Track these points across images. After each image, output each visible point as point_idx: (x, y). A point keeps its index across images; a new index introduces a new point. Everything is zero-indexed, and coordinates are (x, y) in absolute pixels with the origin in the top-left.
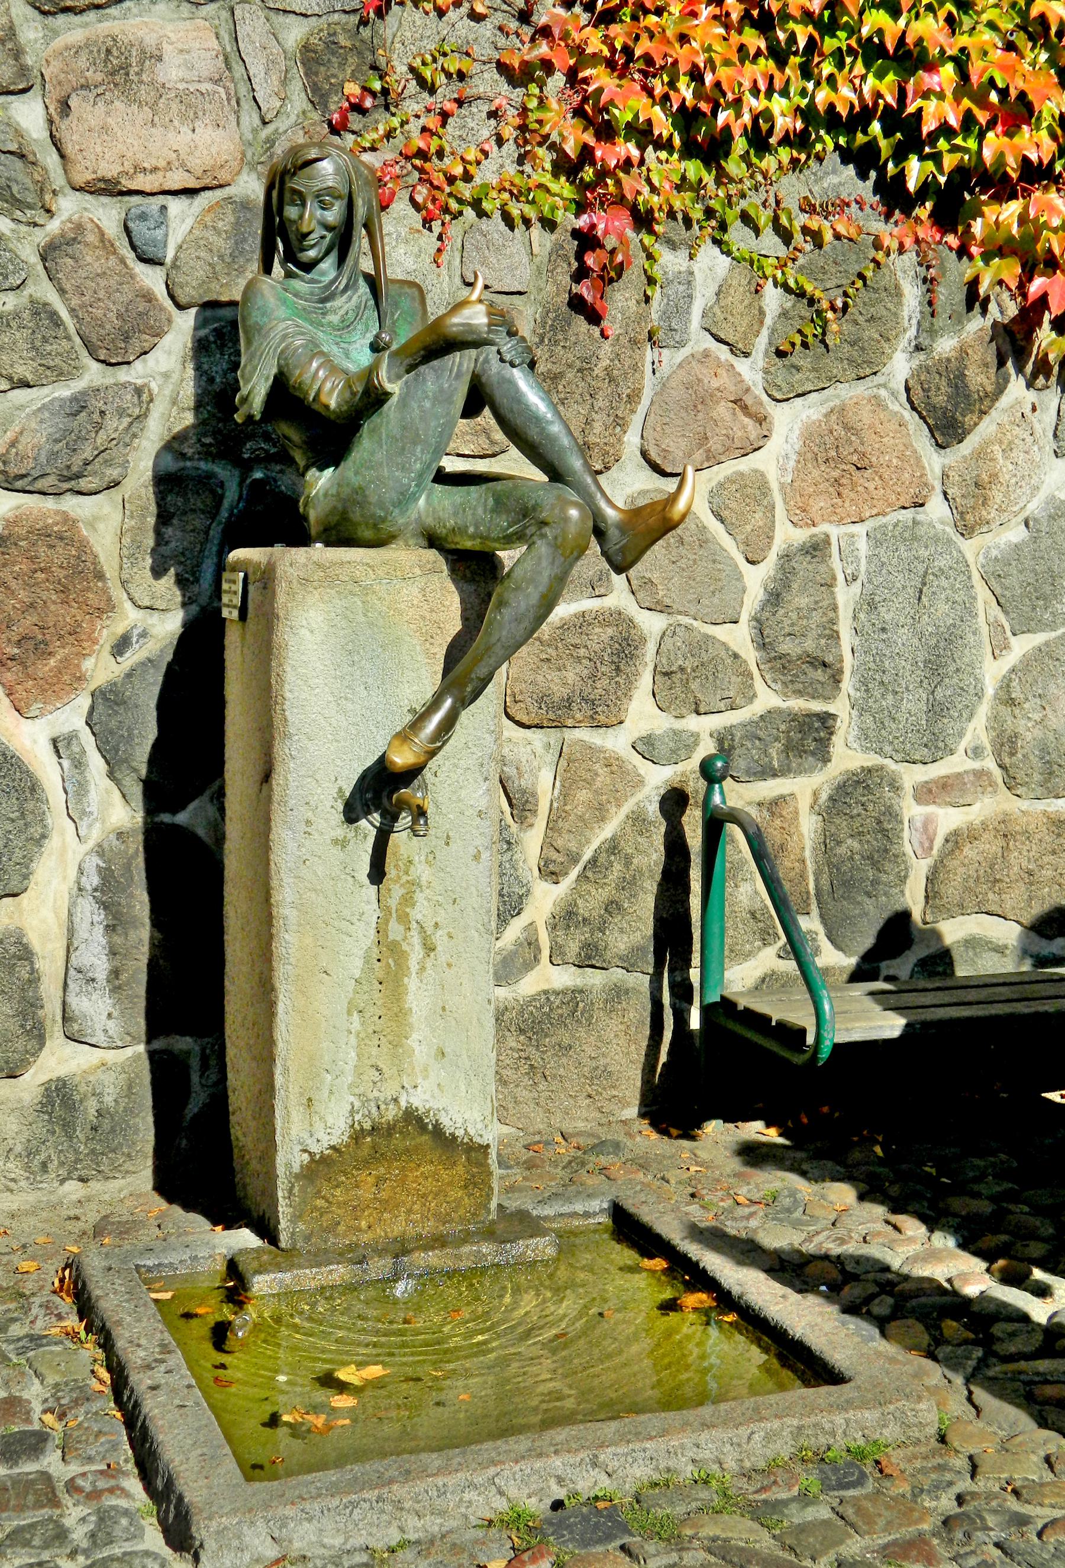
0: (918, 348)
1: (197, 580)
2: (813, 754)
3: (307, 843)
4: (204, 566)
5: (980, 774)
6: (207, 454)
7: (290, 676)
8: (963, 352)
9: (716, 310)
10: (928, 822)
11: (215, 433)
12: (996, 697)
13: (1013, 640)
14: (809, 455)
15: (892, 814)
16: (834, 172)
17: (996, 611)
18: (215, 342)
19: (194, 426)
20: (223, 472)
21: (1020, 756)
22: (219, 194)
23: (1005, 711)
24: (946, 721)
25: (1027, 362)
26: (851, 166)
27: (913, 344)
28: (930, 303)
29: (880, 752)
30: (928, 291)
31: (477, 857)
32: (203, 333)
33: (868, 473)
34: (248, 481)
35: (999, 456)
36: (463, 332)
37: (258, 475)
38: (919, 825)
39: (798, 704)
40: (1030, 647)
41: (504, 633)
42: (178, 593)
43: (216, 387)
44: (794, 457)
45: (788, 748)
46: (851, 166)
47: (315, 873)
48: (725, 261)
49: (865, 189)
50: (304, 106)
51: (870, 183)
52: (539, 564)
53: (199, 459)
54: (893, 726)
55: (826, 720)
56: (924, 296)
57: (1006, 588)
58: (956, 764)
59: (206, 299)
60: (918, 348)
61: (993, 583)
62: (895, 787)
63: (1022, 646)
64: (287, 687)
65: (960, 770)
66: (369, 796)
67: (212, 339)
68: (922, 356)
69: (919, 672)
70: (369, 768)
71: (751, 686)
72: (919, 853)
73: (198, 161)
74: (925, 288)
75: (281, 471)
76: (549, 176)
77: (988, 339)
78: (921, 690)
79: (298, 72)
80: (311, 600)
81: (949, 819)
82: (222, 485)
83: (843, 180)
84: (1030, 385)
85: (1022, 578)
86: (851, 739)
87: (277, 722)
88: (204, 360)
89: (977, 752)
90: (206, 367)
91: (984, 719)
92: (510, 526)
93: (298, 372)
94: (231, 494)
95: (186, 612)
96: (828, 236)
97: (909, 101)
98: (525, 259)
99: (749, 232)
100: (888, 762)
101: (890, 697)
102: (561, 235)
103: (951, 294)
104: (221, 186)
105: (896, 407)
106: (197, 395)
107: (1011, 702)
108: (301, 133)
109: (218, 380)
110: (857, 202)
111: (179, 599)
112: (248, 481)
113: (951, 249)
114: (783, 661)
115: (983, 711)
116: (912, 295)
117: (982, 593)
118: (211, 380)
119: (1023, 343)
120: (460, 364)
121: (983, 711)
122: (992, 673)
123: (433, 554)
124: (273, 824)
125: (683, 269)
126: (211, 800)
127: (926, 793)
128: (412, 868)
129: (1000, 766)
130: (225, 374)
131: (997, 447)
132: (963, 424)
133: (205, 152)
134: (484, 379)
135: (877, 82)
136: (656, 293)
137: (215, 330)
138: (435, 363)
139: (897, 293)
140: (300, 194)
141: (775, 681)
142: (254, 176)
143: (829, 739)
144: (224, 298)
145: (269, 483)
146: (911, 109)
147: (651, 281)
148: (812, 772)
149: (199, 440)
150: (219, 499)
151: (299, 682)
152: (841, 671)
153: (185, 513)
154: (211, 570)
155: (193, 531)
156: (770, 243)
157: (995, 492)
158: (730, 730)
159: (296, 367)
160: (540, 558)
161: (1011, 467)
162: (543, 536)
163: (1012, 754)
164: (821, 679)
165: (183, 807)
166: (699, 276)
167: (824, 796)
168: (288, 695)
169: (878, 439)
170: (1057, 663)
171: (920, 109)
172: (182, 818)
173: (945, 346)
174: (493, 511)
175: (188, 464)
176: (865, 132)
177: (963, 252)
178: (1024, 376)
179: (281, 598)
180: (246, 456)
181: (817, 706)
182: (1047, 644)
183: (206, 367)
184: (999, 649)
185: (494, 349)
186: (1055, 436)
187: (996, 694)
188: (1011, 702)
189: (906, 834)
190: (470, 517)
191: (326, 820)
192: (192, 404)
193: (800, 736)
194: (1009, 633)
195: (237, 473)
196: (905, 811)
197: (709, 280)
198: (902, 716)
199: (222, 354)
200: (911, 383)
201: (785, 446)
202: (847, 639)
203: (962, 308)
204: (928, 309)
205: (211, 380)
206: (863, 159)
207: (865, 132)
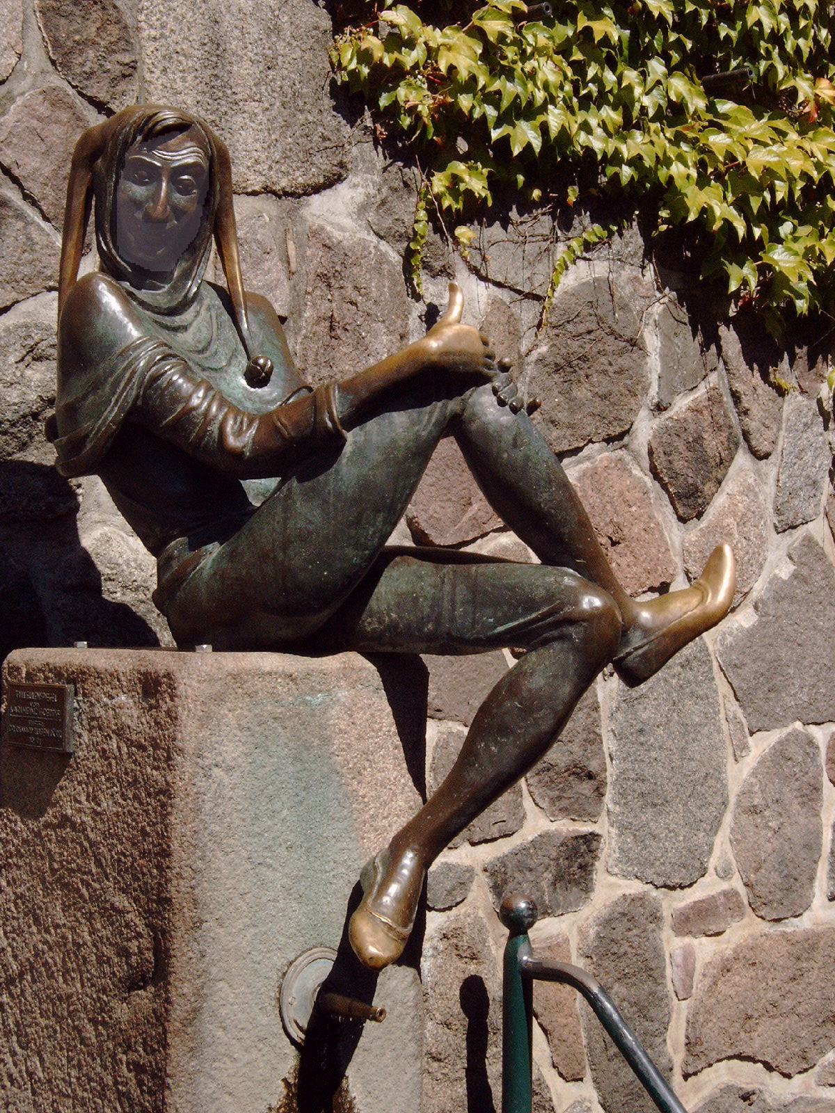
5: (731, 895)
10: (688, 955)
13: (750, 739)
17: (734, 707)
19: (784, 582)
33: (620, 548)
38: (679, 960)
39: (566, 827)
45: (558, 879)
50: (43, 65)
55: (594, 837)
58: (707, 888)
61: (730, 674)
62: (656, 918)
63: (761, 745)
71: (521, 805)
79: (36, 21)
81: (706, 949)
85: (755, 667)
89: (725, 874)
98: (283, 276)
105: (637, 472)
114: (552, 773)
117: (722, 687)
127: (690, 922)
129: (746, 885)
141: (543, 798)
143: (593, 865)
152: (603, 783)
158: (503, 861)
164: (586, 792)
169: (627, 509)
181: (585, 828)
182: (780, 743)
184: (741, 749)
189: (668, 972)
193: (566, 863)
194: (748, 734)
196: (665, 944)
202: (609, 744)
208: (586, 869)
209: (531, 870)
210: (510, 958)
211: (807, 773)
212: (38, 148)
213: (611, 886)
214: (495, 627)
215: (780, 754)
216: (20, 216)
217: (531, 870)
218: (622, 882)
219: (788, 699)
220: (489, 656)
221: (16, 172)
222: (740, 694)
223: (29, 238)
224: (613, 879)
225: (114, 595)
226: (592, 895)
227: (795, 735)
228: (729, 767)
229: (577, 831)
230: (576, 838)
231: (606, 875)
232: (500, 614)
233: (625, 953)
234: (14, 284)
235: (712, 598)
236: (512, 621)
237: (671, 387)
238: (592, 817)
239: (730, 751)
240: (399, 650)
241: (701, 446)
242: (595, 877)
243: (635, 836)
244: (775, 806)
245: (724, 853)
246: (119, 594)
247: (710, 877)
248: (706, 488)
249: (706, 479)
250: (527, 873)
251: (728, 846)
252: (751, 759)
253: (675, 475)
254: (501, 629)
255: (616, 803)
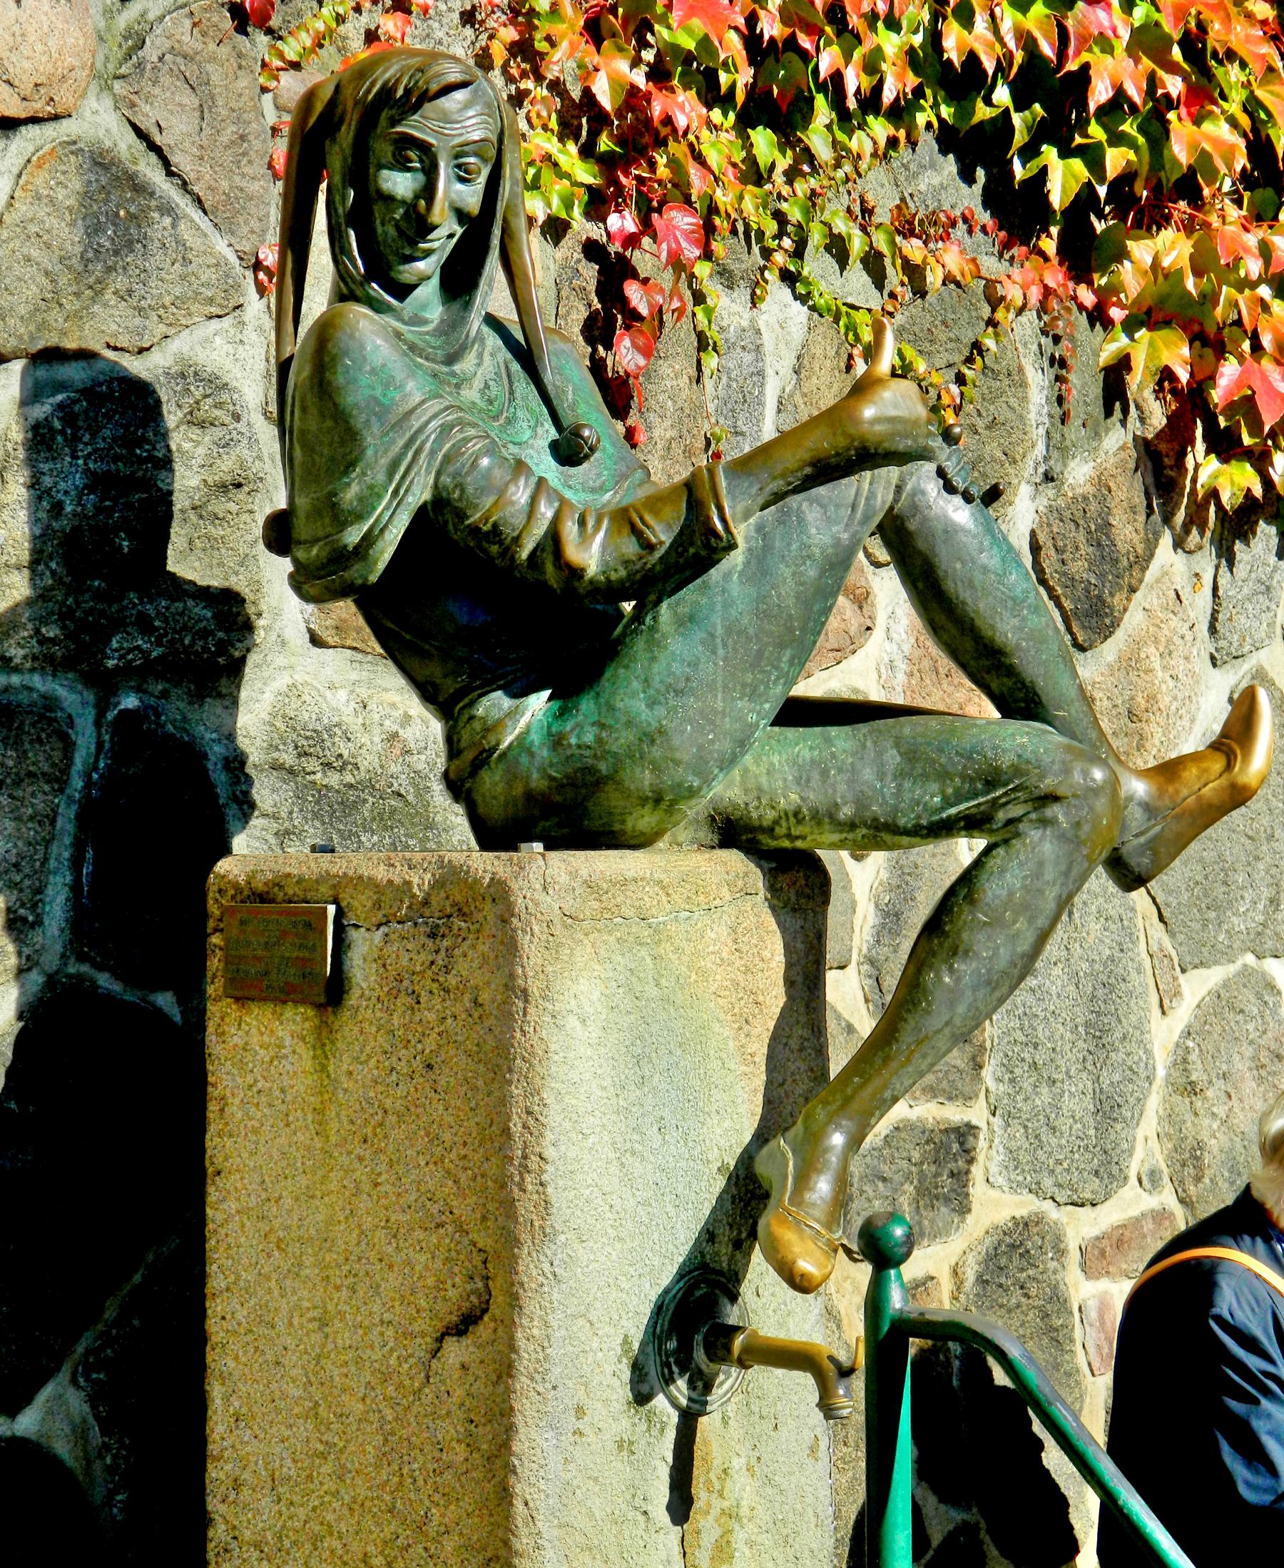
0: (1048, 478)
1: (38, 922)
2: (947, 1200)
3: (578, 1452)
4: (50, 891)
6: (47, 662)
7: (554, 1117)
8: (1102, 485)
9: (798, 399)
11: (64, 617)
12: (1169, 1081)
13: (1182, 979)
14: (926, 663)
15: (1058, 1299)
16: (933, 166)
18: (63, 432)
19: (29, 602)
20: (70, 696)
21: (1207, 1180)
22: (49, 132)
23: (1182, 1103)
24: (1118, 1127)
25: (1177, 505)
26: (951, 156)
27: (1041, 470)
28: (1060, 400)
29: (1036, 1190)
30: (1058, 378)
31: (813, 1450)
32: (41, 411)
34: (110, 716)
35: (1156, 663)
36: (893, 435)
37: (130, 702)
38: (1093, 1314)
40: (1204, 992)
41: (961, 1009)
42: (11, 948)
43: (63, 524)
44: (902, 666)
46: (951, 156)
47: (591, 1515)
48: (799, 312)
49: (969, 198)
51: (978, 188)
52: (1038, 874)
53: (32, 670)
54: (1054, 1141)
55: (965, 1133)
56: (1052, 387)
57: (1170, 892)
59: (41, 345)
60: (1048, 478)
63: (1197, 986)
64: (549, 1136)
65: (1134, 1212)
66: (672, 1345)
67: (57, 424)
68: (1050, 490)
69: (1081, 1044)
70: (666, 1291)
72: (1096, 1366)
73: (27, 65)
74: (1051, 373)
75: (165, 695)
76: (555, 139)
77: (1132, 465)
78: (1084, 1075)
80: (583, 954)
82: (70, 721)
83: (941, 183)
84: (1178, 544)
86: (994, 1169)
87: (525, 1208)
88: (45, 467)
89: (1151, 1180)
90: (47, 481)
91: (1155, 1121)
92: (947, 803)
93: (488, 502)
94: (85, 739)
95: (22, 986)
96: (934, 278)
97: (1071, 51)
99: (830, 263)
100: (1048, 1206)
101: (1044, 1090)
102: (570, 248)
103: (1085, 387)
104: (56, 117)
106: (34, 539)
107: (1192, 1089)
108: (188, 23)
109: (69, 509)
110: (965, 220)
111: (13, 961)
112: (110, 716)
113: (1081, 307)
115: (1154, 1103)
116: (1038, 382)
118: (57, 508)
119: (1172, 473)
120: (872, 495)
121: (1154, 1103)
122: (1163, 1034)
123: (734, 859)
124: (518, 1420)
125: (745, 324)
126: (74, 1381)
128: (729, 1483)
129: (1182, 1201)
130: (80, 497)
131: (1152, 650)
132: (1111, 608)
133: (39, 47)
134: (912, 525)
135: (1019, 16)
136: (711, 361)
137: (60, 406)
138: (821, 491)
139: (1017, 379)
140: (425, 149)
142: (108, 102)
143: (968, 1172)
144: (70, 344)
145: (147, 717)
146: (1072, 66)
147: (703, 343)
148: (948, 1234)
149: (37, 631)
150: (68, 747)
151: (567, 1125)
153: (18, 783)
154: (61, 899)
155: (31, 818)
156: (857, 284)
157: (1153, 727)
159: (482, 491)
160: (1041, 864)
161: (1171, 683)
162: (1044, 823)
163: (1198, 1179)
164: (959, 1063)
165: (27, 1400)
166: (768, 339)
167: (970, 1275)
168: (550, 1153)
170: (1239, 1018)
171: (1086, 67)
172: (27, 1423)
173: (1079, 474)
174: (900, 775)
175: (15, 679)
176: (988, 102)
177: (1098, 316)
178: (1172, 528)
179: (532, 951)
180: (111, 663)
181: (954, 1114)
182: (1226, 984)
183: (47, 481)
185: (930, 467)
186: (1213, 630)
187: (1169, 1075)
188: (1192, 1089)
190: (842, 788)
191: (606, 1402)
192: (25, 557)
193: (933, 1168)
195: (90, 697)
196: (1072, 1291)
197: (782, 346)
198: (1064, 1124)
199: (75, 457)
200: (1042, 538)
201: (887, 645)
203: (1098, 410)
204: (1057, 411)
205: (57, 508)
206: (975, 148)
207: (988, 102)
208: (961, 1178)
209: (884, 1180)
210: (874, 1303)
211: (1265, 1032)
212: (186, 101)
213: (995, 1202)
214: (943, 809)
215: (1221, 1003)
216: (167, 209)
217: (884, 1180)
218: (1008, 1197)
219: (1235, 920)
220: (943, 845)
221: (158, 139)
222: (1165, 914)
223: (180, 242)
224: (994, 1194)
225: (312, 777)
226: (970, 1219)
227: (1246, 971)
228: (1153, 1025)
229: (947, 1121)
230: (946, 1130)
231: (985, 1187)
232: (950, 791)
233: (1018, 1306)
234: (161, 312)
235: (1241, 769)
236: (968, 799)
237: (1058, 447)
238: (968, 1098)
239: (1154, 999)
240: (799, 844)
241: (1108, 537)
242: (971, 1190)
243: (1026, 1127)
244: (1220, 1084)
245: (1149, 1153)
246: (319, 775)
247: (1130, 1191)
248: (1116, 600)
249: (1116, 587)
250: (880, 1184)
251: (1154, 1143)
252: (1183, 1013)
253: (1071, 582)
254: (953, 811)
255: (999, 1080)
